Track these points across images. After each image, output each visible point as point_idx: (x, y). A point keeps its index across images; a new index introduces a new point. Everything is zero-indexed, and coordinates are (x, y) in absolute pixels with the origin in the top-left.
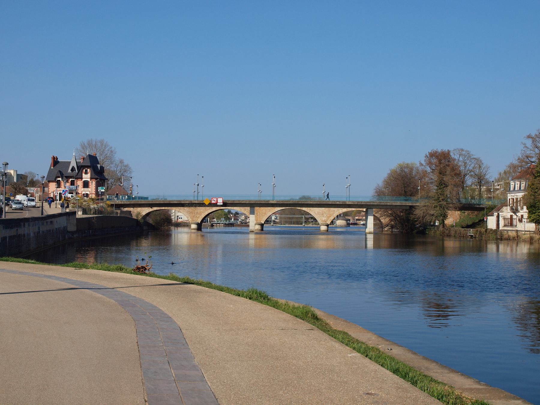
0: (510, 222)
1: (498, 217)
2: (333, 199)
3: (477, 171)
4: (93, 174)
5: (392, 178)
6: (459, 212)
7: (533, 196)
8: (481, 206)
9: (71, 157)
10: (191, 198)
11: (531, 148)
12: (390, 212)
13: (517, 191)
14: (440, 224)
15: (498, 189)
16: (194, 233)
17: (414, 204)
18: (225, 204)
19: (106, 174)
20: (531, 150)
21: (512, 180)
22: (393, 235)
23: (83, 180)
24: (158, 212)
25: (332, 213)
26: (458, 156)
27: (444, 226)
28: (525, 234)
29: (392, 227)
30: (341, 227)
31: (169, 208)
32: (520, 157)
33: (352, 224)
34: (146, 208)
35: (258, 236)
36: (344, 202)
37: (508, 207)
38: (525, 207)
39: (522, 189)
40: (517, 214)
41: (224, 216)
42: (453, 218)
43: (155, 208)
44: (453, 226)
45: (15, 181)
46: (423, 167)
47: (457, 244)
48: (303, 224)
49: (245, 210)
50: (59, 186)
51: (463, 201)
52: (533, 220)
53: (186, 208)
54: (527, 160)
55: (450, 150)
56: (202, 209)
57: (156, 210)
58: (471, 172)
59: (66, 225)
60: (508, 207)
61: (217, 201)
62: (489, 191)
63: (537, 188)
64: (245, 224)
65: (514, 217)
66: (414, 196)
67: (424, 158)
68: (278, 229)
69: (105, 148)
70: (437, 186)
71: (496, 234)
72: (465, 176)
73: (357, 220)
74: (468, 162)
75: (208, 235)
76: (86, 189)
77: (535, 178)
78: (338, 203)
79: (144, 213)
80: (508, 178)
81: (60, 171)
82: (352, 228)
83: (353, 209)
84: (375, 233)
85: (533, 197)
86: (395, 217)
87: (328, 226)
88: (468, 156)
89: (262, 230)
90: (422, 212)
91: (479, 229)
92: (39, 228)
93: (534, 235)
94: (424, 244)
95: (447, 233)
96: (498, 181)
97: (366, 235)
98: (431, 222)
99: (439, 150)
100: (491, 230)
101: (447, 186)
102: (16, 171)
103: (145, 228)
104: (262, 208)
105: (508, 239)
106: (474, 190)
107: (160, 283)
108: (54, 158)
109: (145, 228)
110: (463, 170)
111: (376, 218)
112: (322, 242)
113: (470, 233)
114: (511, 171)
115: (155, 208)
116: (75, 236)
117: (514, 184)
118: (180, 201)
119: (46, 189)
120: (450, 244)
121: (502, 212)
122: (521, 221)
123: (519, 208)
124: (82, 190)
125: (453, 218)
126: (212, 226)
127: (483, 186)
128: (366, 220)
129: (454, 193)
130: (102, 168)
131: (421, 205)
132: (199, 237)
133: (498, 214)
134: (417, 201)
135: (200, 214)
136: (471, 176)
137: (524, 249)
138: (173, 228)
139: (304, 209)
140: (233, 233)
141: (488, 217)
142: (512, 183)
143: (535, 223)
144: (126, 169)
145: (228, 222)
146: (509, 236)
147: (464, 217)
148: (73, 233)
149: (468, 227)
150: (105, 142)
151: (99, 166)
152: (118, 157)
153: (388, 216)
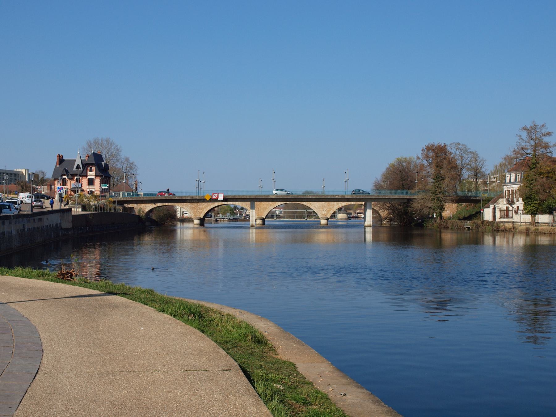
0: (507, 214)
1: (494, 209)
2: (329, 193)
3: (473, 164)
4: (98, 172)
5: (390, 172)
6: (456, 205)
7: (529, 187)
8: (478, 198)
9: (77, 156)
10: (194, 195)
11: (526, 140)
12: (388, 205)
13: (513, 183)
14: (437, 216)
15: (494, 182)
16: (197, 228)
17: (412, 198)
18: (226, 199)
19: (111, 172)
20: (526, 142)
21: (508, 172)
22: (391, 228)
23: (88, 177)
24: (161, 208)
25: (332, 207)
26: (455, 150)
27: (441, 219)
28: (521, 225)
29: (391, 220)
30: (342, 220)
31: (172, 204)
32: (516, 149)
33: (353, 217)
34: (150, 204)
35: (260, 230)
36: (343, 196)
37: (504, 199)
38: (521, 199)
39: (517, 180)
40: (513, 206)
41: (226, 211)
42: (450, 210)
43: (158, 205)
44: (450, 219)
45: (27, 179)
46: (420, 161)
47: (455, 236)
48: (306, 218)
49: (247, 205)
50: (64, 183)
51: (460, 194)
52: (529, 211)
53: (188, 204)
54: (523, 152)
55: (447, 144)
56: (204, 204)
57: (160, 206)
58: (467, 165)
59: (59, 222)
60: (504, 199)
61: (218, 196)
62: (485, 183)
63: (532, 180)
64: (247, 218)
65: (510, 208)
66: (412, 189)
67: (421, 152)
68: (282, 223)
69: (111, 146)
70: (434, 179)
71: (493, 226)
72: (461, 169)
73: (358, 213)
74: (464, 155)
75: (213, 230)
76: (91, 186)
77: (531, 170)
78: (337, 197)
79: (147, 210)
80: (504, 170)
81: (65, 170)
82: (353, 222)
83: (353, 203)
84: (373, 226)
85: (528, 189)
86: (393, 210)
87: (328, 219)
88: (465, 149)
89: (263, 224)
90: (419, 205)
91: (476, 221)
92: (24, 226)
93: (530, 227)
94: (422, 236)
95: (444, 225)
96: (494, 173)
97: (365, 228)
98: (429, 214)
99: (436, 144)
100: (488, 222)
101: (444, 179)
102: (28, 170)
103: (148, 224)
104: (263, 203)
105: (505, 231)
106: (470, 183)
107: (74, 294)
108: (59, 156)
109: (148, 224)
110: (459, 163)
111: (374, 212)
112: (322, 237)
113: (467, 225)
114: (507, 163)
115: (158, 205)
116: (70, 233)
117: (510, 176)
118: (181, 197)
119: (53, 187)
120: (448, 237)
121: (498, 204)
122: (516, 212)
123: (515, 199)
124: (87, 188)
125: (450, 210)
126: (217, 221)
127: (480, 179)
128: (365, 214)
129: (451, 186)
130: (106, 165)
131: (420, 199)
132: (202, 233)
133: (495, 206)
134: (415, 194)
135: (202, 209)
136: (468, 169)
137: (520, 241)
138: (179, 224)
139: (304, 203)
140: (237, 227)
141: (485, 209)
142: (508, 175)
143: (531, 214)
144: (132, 166)
145: (231, 217)
146: (505, 228)
147: (461, 209)
148: (67, 230)
149: (465, 219)
150: (111, 141)
151: (103, 163)
152: (123, 155)
153: (386, 209)
